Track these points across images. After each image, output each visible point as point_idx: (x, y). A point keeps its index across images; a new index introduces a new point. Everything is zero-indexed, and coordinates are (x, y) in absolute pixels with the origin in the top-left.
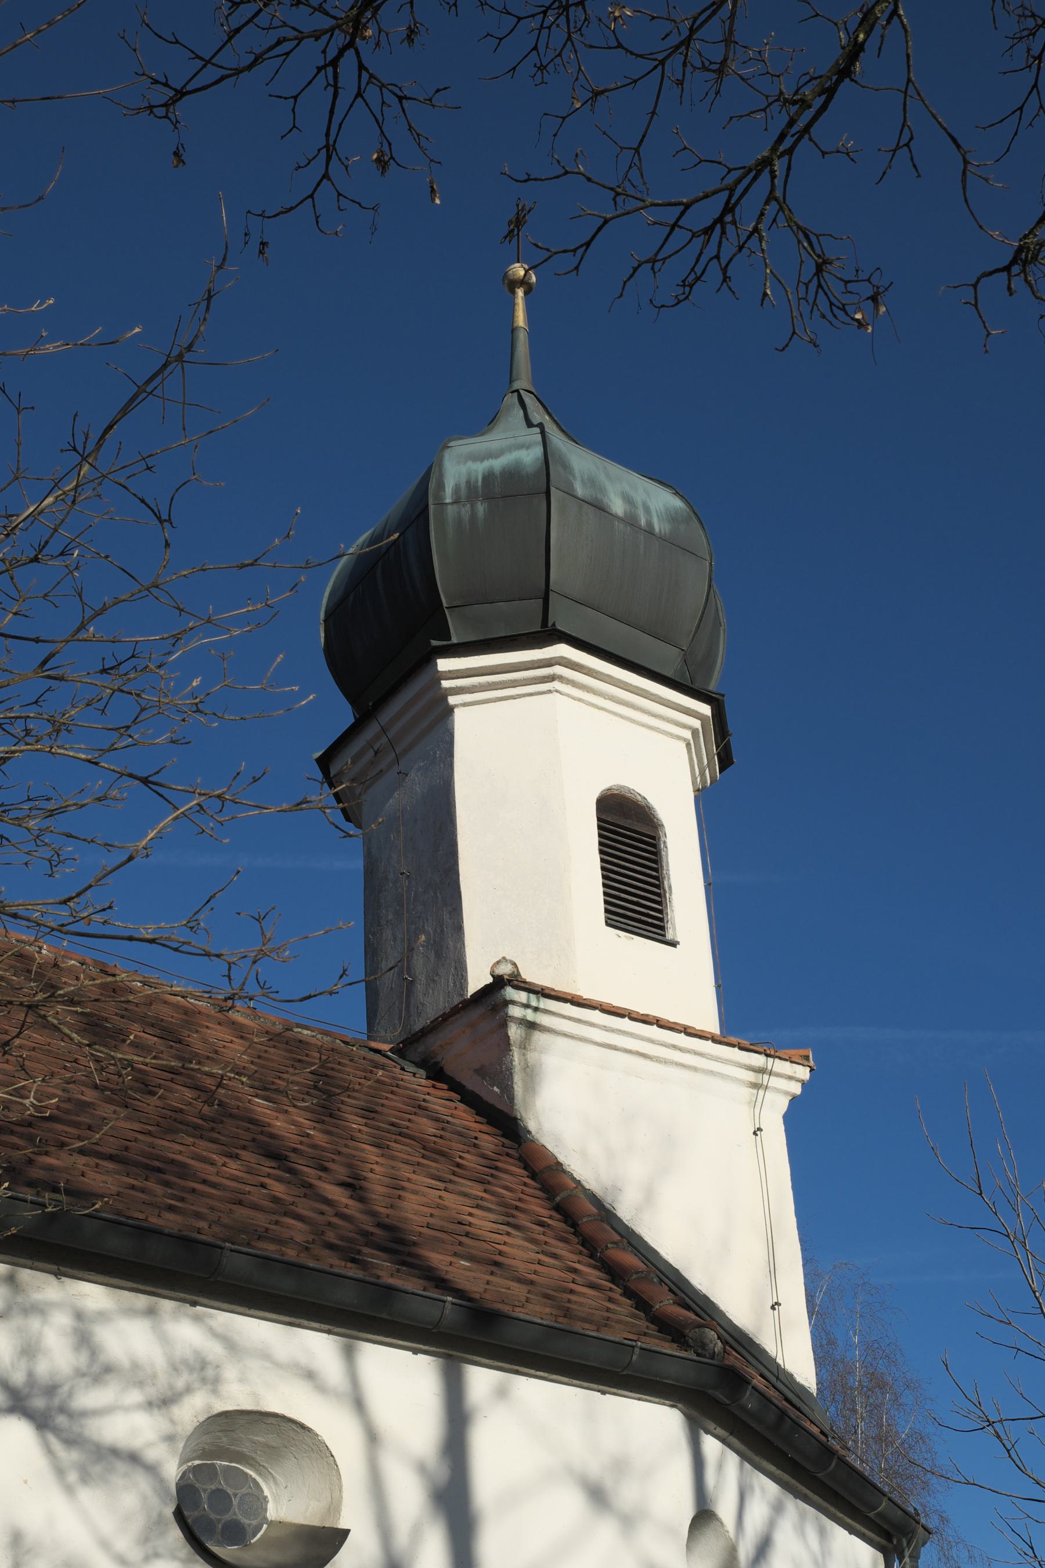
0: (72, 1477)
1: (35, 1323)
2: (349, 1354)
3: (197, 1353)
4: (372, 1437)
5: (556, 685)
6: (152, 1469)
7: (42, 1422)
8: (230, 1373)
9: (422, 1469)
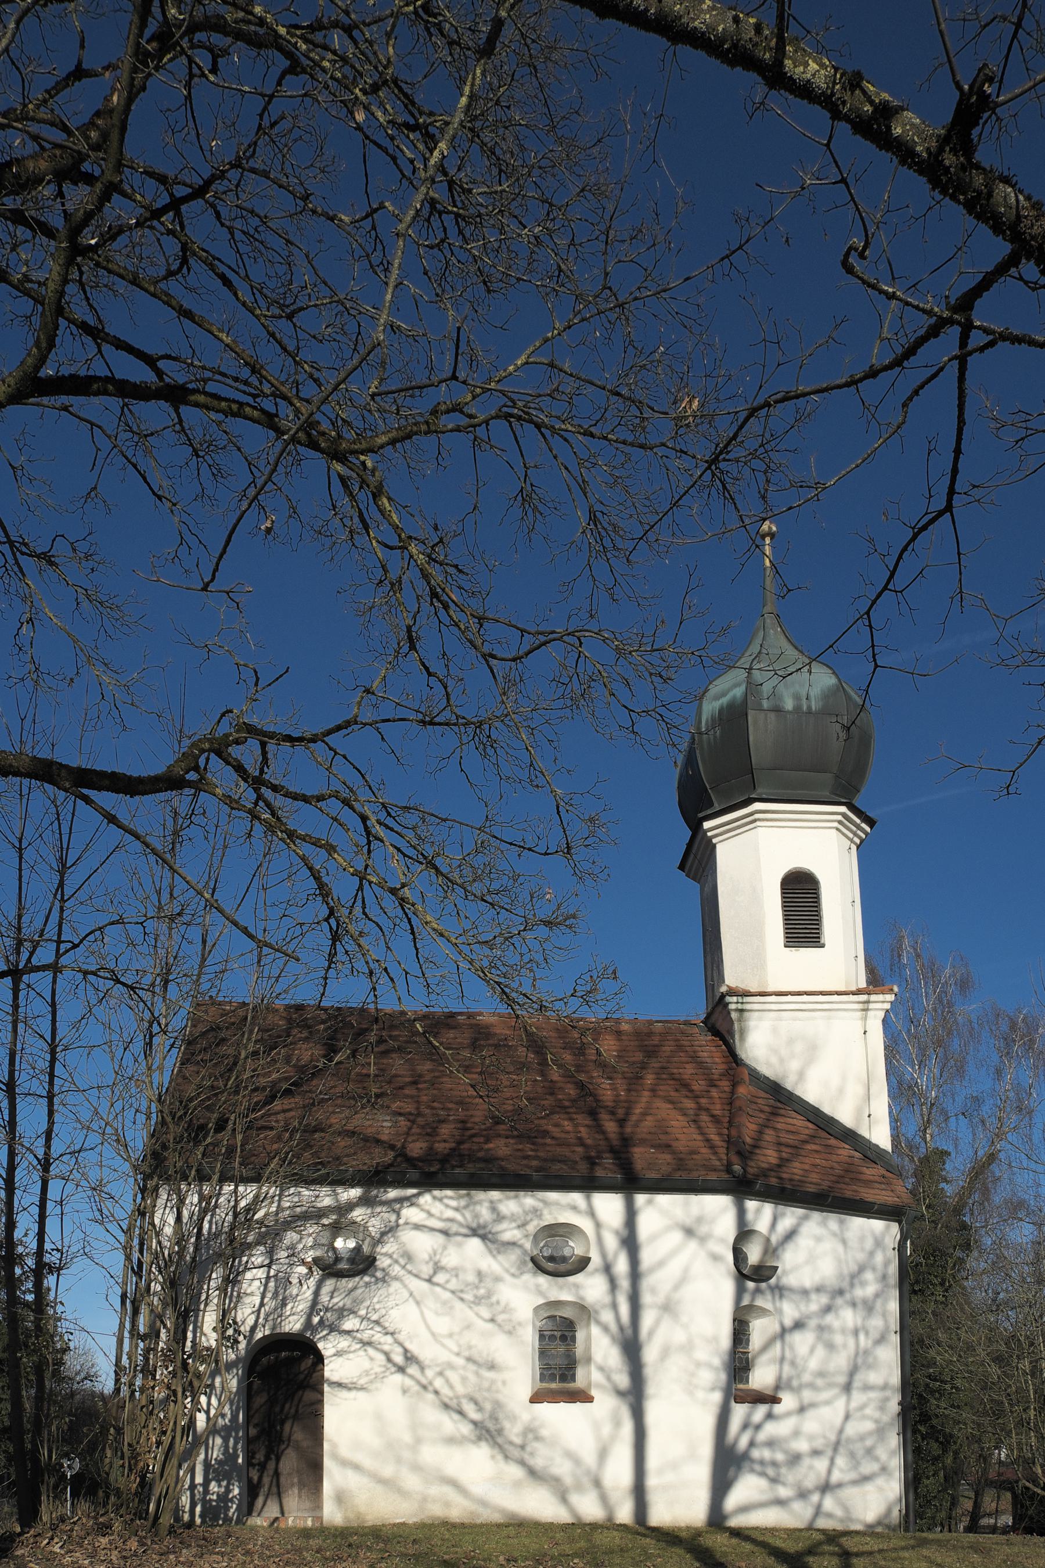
0: (495, 1252)
1: (478, 1208)
2: (588, 1198)
3: (534, 1207)
4: (598, 1225)
5: (758, 823)
6: (521, 1246)
7: (484, 1238)
8: (545, 1212)
9: (617, 1233)
